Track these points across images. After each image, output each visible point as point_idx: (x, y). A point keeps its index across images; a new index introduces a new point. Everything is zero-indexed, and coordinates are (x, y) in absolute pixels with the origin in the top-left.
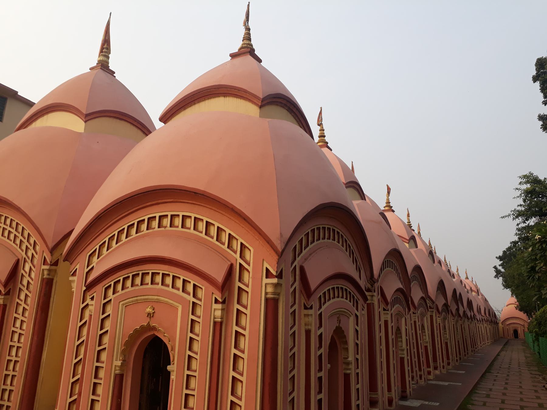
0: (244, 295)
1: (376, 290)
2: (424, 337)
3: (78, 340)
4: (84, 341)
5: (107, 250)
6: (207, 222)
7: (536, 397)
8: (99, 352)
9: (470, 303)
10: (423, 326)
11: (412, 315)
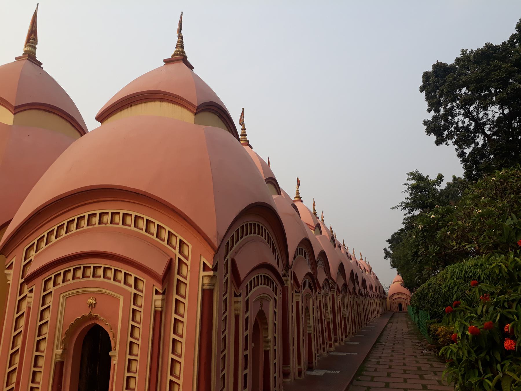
0: (182, 287)
1: (290, 275)
2: (327, 314)
3: (15, 330)
4: (21, 332)
5: (46, 244)
6: (147, 220)
7: (416, 361)
8: (39, 342)
9: (364, 281)
10: (326, 304)
11: (318, 295)
